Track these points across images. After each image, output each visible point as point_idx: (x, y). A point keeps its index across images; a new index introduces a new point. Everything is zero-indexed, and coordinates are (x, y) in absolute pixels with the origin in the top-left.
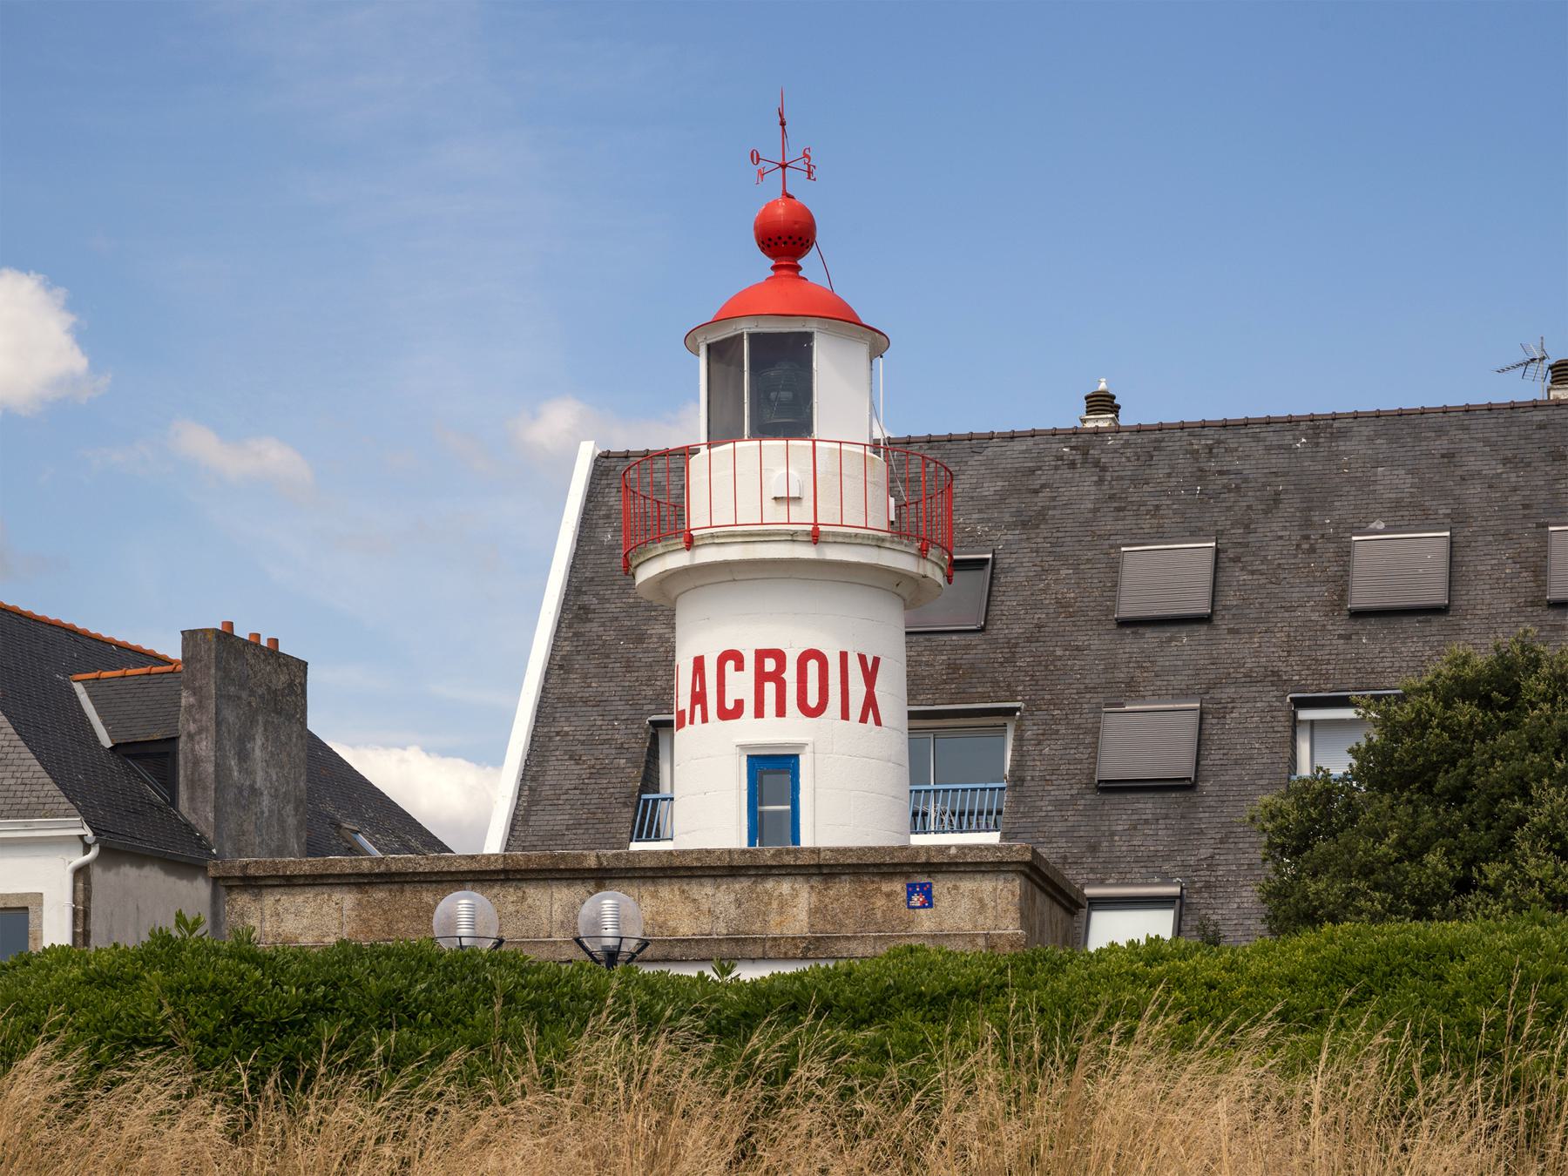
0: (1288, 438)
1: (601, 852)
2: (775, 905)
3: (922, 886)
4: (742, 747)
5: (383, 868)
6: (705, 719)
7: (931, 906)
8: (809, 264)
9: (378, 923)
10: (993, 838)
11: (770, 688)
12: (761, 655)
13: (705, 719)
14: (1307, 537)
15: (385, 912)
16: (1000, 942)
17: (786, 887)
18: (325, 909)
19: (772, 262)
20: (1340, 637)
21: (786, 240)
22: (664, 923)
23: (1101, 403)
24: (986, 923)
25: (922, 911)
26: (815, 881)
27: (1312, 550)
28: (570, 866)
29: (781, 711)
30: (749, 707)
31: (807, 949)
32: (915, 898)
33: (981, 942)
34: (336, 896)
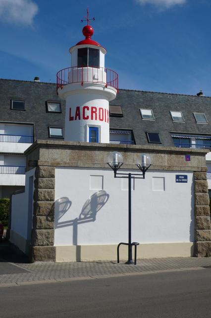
6: (79, 119)
10: (118, 143)
11: (94, 114)
12: (92, 108)
17: (163, 155)
21: (87, 32)
23: (36, 78)
30: (74, 118)
34: (66, 150)
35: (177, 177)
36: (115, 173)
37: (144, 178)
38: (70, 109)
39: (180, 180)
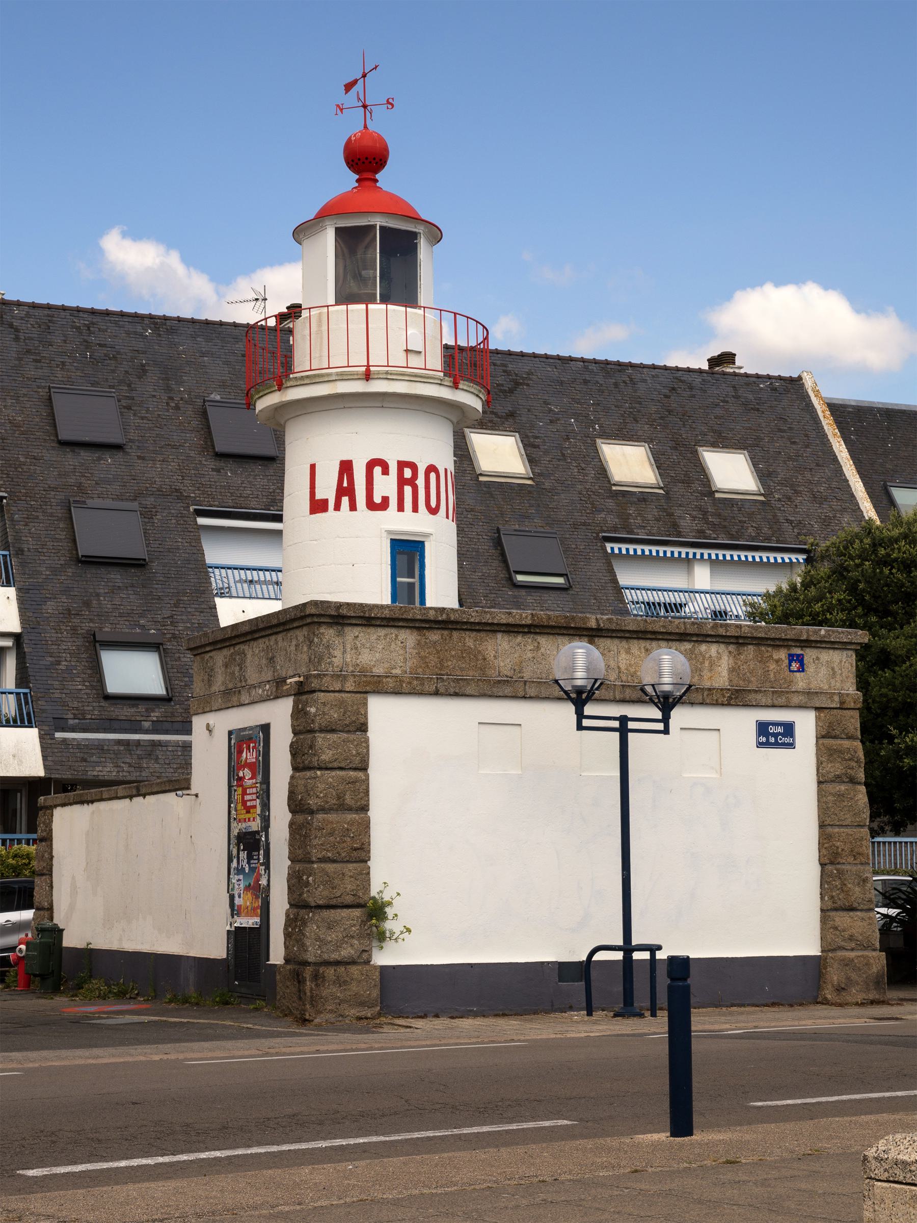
0: (139, 329)
1: (598, 616)
2: (707, 664)
3: (798, 656)
4: (389, 532)
5: (444, 617)
6: (353, 507)
7: (803, 671)
8: (386, 179)
9: (433, 660)
11: (408, 490)
12: (402, 465)
13: (353, 507)
14: (171, 398)
15: (438, 652)
16: (848, 699)
18: (393, 646)
19: (357, 177)
20: (213, 470)
21: (366, 159)
22: (635, 672)
24: (837, 684)
25: (798, 674)
26: (732, 648)
27: (177, 408)
28: (578, 625)
29: (415, 509)
30: (393, 502)
31: (730, 698)
32: (794, 664)
33: (836, 698)
35: (763, 728)
36: (580, 716)
37: (666, 731)
38: (313, 467)
39: (772, 740)
